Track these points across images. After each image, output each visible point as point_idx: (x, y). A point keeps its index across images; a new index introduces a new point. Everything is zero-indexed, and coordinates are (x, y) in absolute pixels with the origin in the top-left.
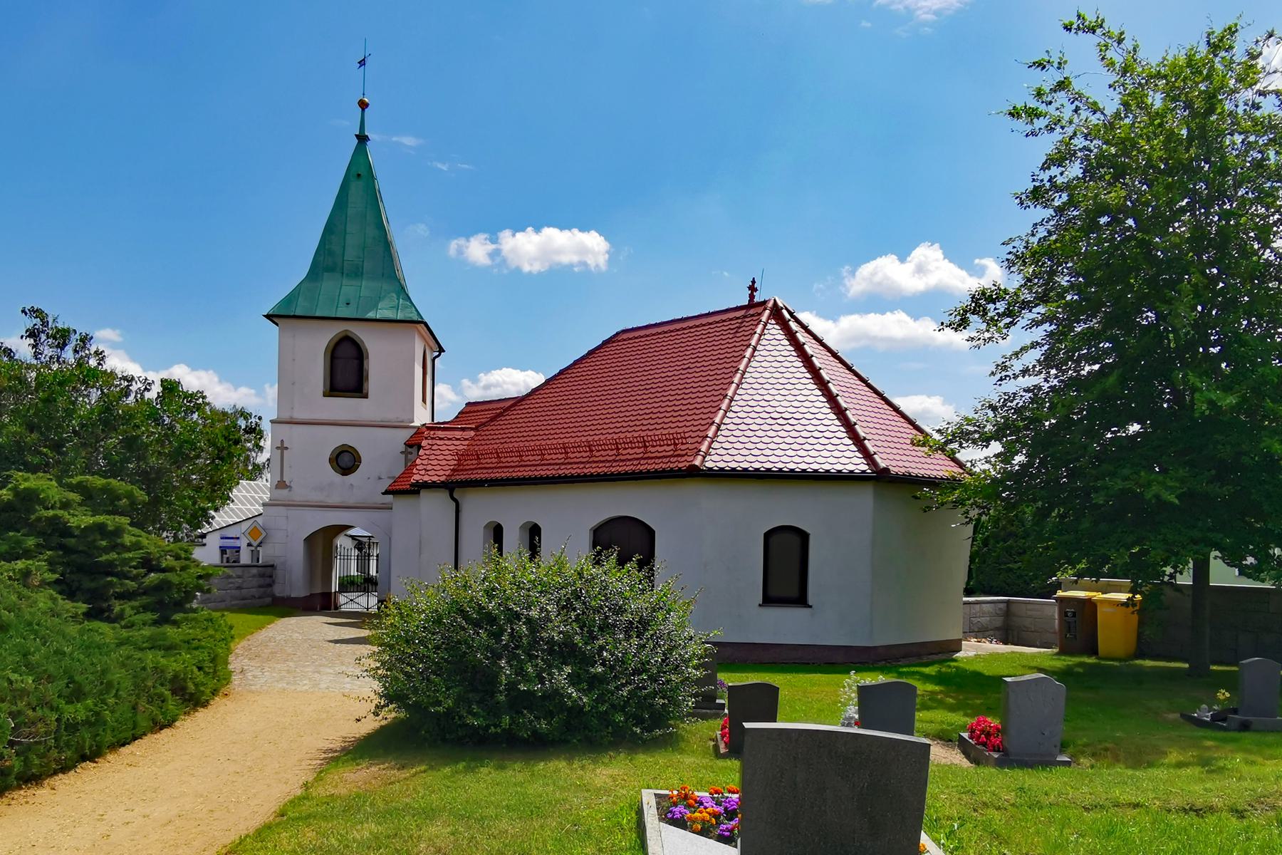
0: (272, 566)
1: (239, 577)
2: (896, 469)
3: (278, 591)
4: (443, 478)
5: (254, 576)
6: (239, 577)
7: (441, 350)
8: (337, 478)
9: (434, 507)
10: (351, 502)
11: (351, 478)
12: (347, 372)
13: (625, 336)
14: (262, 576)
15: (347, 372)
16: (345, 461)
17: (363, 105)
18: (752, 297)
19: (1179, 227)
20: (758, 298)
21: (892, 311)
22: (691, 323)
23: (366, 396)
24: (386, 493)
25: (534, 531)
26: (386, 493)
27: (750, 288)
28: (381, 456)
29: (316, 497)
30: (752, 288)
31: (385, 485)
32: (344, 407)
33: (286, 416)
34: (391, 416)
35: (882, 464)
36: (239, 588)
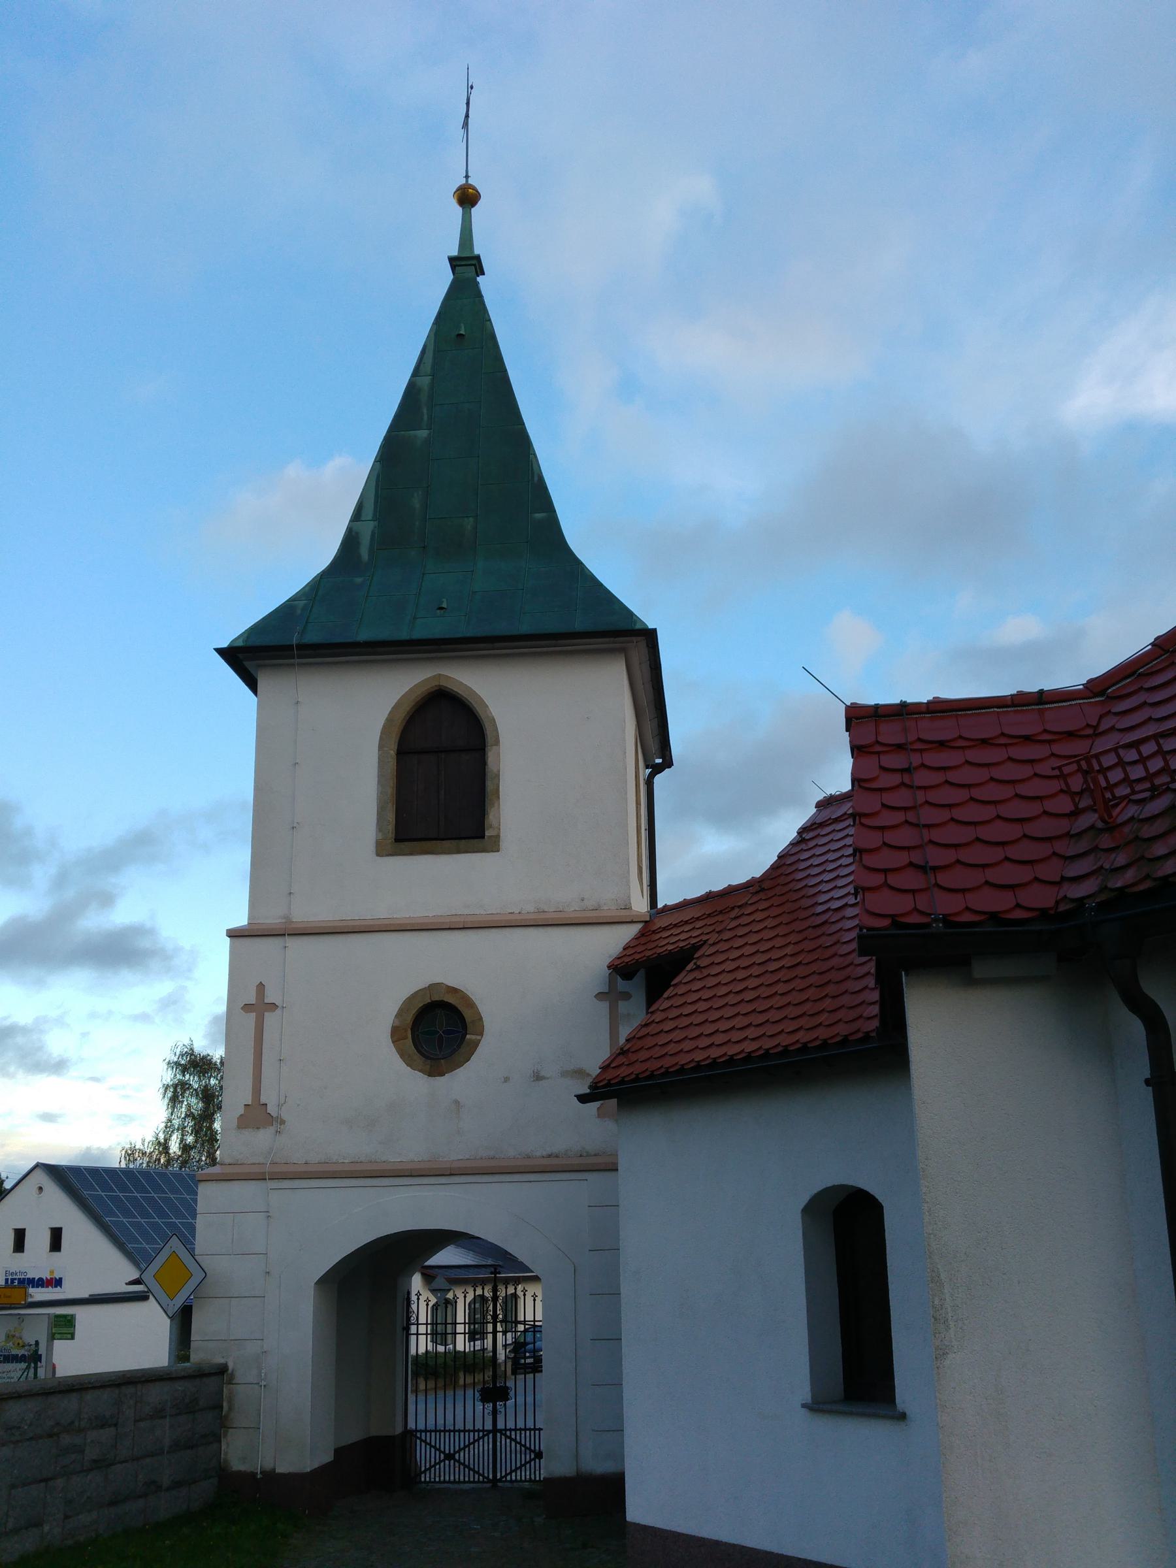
1: (102, 1423)
3: (243, 1452)
5: (159, 1413)
6: (102, 1423)
8: (413, 1083)
10: (455, 1154)
11: (462, 1082)
12: (440, 788)
15: (440, 788)
16: (438, 1029)
17: (467, 198)
23: (494, 846)
28: (543, 993)
29: (351, 1147)
32: (439, 880)
33: (272, 917)
34: (565, 895)
36: (100, 1464)
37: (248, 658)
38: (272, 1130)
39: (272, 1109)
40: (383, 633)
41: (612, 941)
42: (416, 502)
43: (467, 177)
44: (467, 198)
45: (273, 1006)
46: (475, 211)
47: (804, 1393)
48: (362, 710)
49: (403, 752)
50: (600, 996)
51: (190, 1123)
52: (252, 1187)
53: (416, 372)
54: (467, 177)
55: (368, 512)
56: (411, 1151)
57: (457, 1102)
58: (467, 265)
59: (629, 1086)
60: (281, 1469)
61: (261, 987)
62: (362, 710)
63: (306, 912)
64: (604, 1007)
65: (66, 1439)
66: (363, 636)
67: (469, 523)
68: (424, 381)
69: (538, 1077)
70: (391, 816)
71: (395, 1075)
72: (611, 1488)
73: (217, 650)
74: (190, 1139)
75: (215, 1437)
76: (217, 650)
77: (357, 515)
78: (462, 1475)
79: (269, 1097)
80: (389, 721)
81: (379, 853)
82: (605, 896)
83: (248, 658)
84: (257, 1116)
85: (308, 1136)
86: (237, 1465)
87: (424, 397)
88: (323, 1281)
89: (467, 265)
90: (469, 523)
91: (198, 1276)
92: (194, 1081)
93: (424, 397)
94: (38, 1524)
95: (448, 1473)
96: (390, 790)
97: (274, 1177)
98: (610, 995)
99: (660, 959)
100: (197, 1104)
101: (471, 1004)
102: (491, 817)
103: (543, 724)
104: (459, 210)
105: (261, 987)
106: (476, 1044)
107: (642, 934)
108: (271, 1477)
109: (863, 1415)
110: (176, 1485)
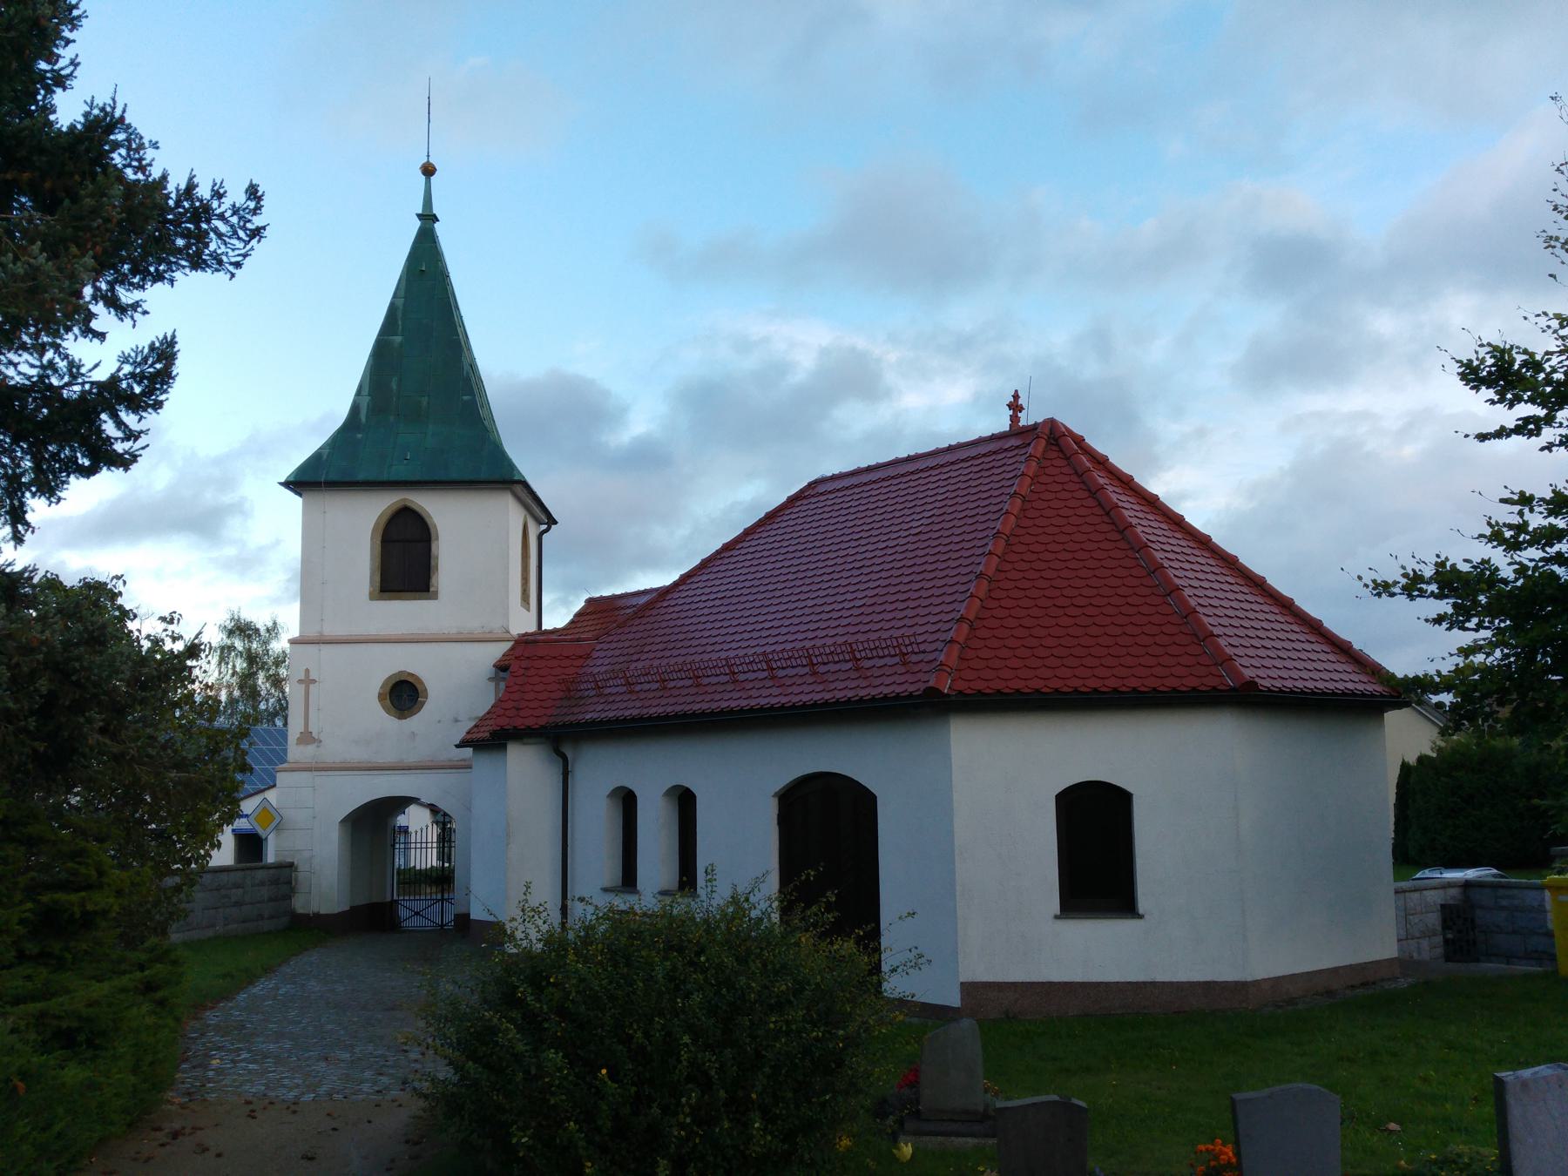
0: (291, 865)
1: (237, 886)
2: (1267, 683)
3: (300, 905)
4: (542, 722)
5: (262, 884)
6: (237, 886)
7: (552, 521)
8: (389, 722)
9: (525, 768)
10: (412, 759)
11: (415, 722)
12: (405, 562)
13: (821, 489)
14: (275, 882)
15: (405, 562)
16: (404, 695)
17: (428, 171)
18: (1014, 419)
19: (690, 1098)
20: (1025, 420)
21: (53, 584)
22: (921, 465)
23: (435, 596)
24: (463, 744)
25: (685, 801)
26: (463, 744)
27: (1010, 406)
28: (461, 682)
29: (358, 754)
30: (1015, 407)
31: (460, 734)
32: (404, 613)
33: (312, 633)
34: (474, 625)
35: (1248, 673)
36: (238, 904)
37: (297, 484)
40: (371, 478)
41: (498, 650)
42: (394, 386)
44: (428, 171)
45: (314, 681)
47: (1055, 905)
48: (362, 516)
49: (383, 541)
50: (490, 679)
51: (234, 681)
52: (305, 774)
53: (395, 296)
55: (366, 391)
56: (389, 757)
58: (428, 218)
59: (490, 738)
60: (322, 912)
61: (307, 671)
62: (362, 516)
63: (330, 630)
64: (493, 684)
65: (223, 892)
66: (361, 477)
67: (425, 401)
68: (400, 302)
69: (456, 721)
70: (378, 578)
72: (468, 915)
74: (236, 693)
75: (288, 897)
77: (359, 393)
78: (425, 922)
79: (313, 728)
80: (377, 524)
81: (372, 599)
82: (495, 625)
83: (297, 484)
84: (307, 738)
85: (334, 749)
86: (300, 911)
87: (400, 314)
88: (344, 821)
89: (428, 218)
90: (425, 401)
91: (278, 819)
92: (239, 645)
93: (400, 314)
94: (213, 926)
95: (416, 922)
96: (378, 560)
97: (317, 769)
98: (494, 680)
99: (529, 658)
100: (240, 665)
101: (422, 683)
102: (433, 580)
103: (463, 526)
105: (307, 671)
107: (512, 649)
108: (317, 916)
110: (271, 917)
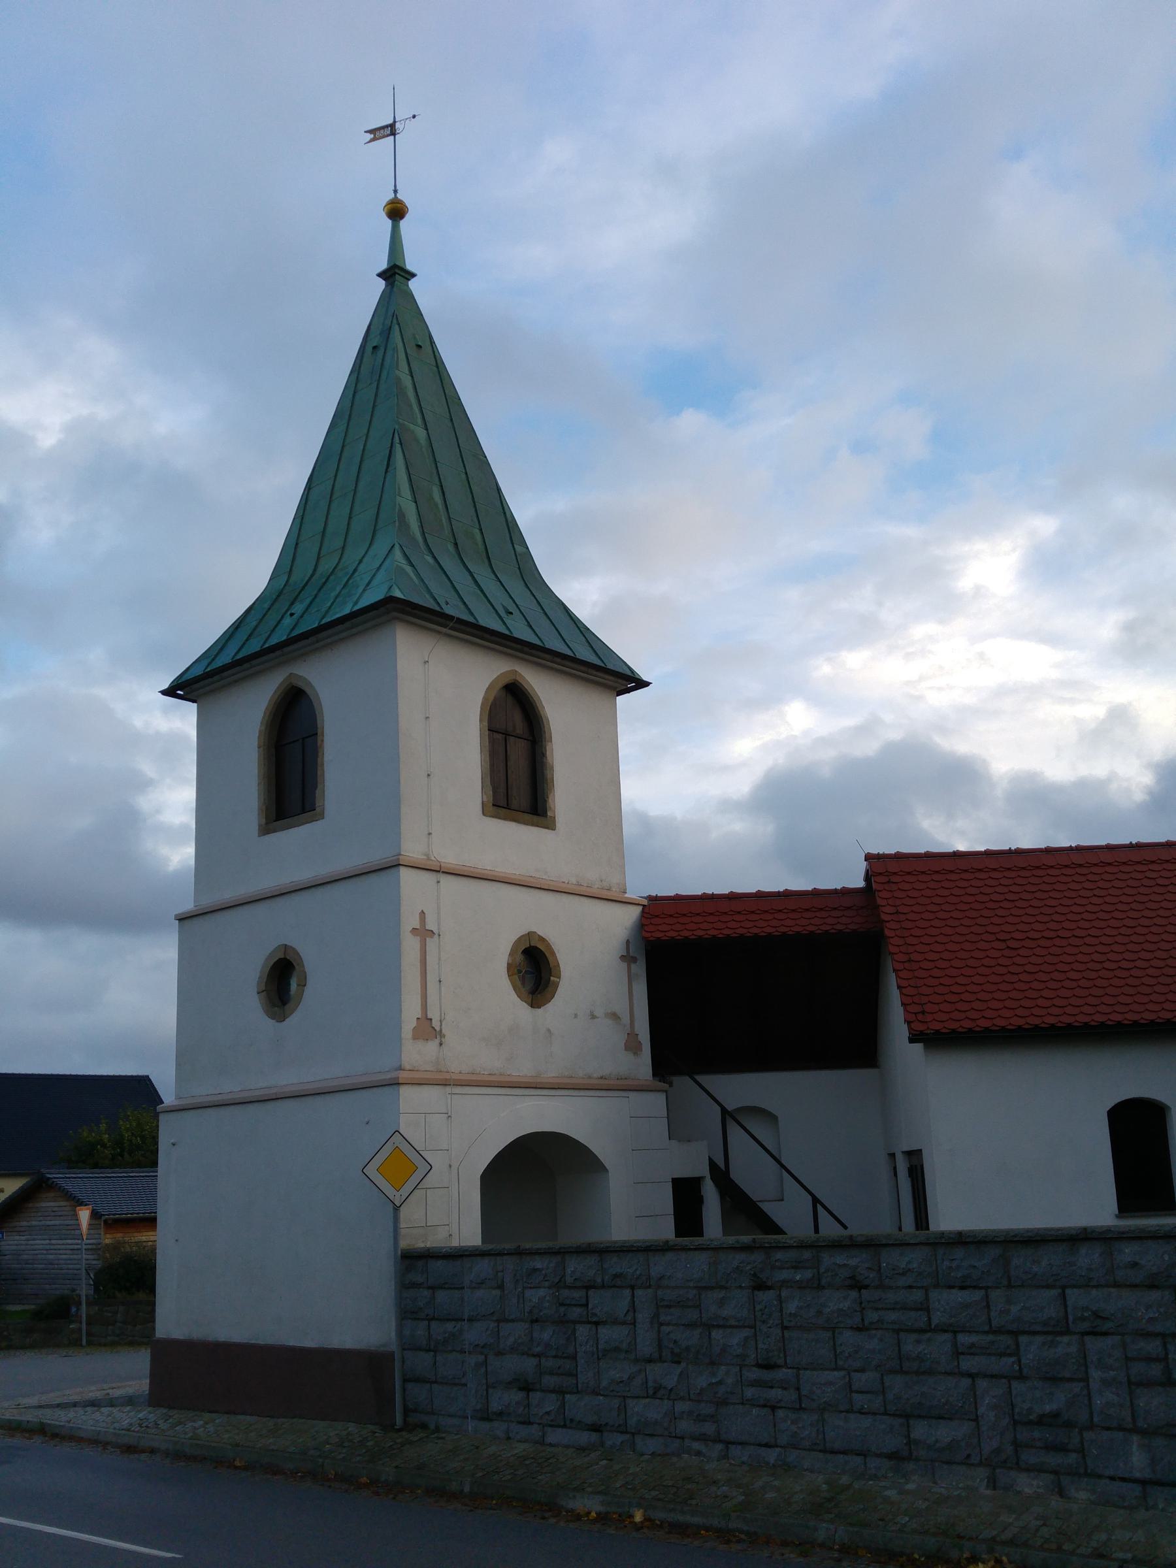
10: (551, 1073)
17: (396, 212)
38: (437, 1041)
39: (436, 1024)
43: (395, 191)
44: (396, 212)
46: (403, 224)
50: (623, 958)
54: (395, 191)
56: (523, 1069)
57: (549, 1030)
58: (396, 274)
64: (625, 965)
69: (593, 1017)
71: (503, 997)
73: (642, 684)
76: (642, 684)
79: (433, 1014)
89: (396, 274)
104: (389, 223)
106: (556, 985)
109: (212, 691)
